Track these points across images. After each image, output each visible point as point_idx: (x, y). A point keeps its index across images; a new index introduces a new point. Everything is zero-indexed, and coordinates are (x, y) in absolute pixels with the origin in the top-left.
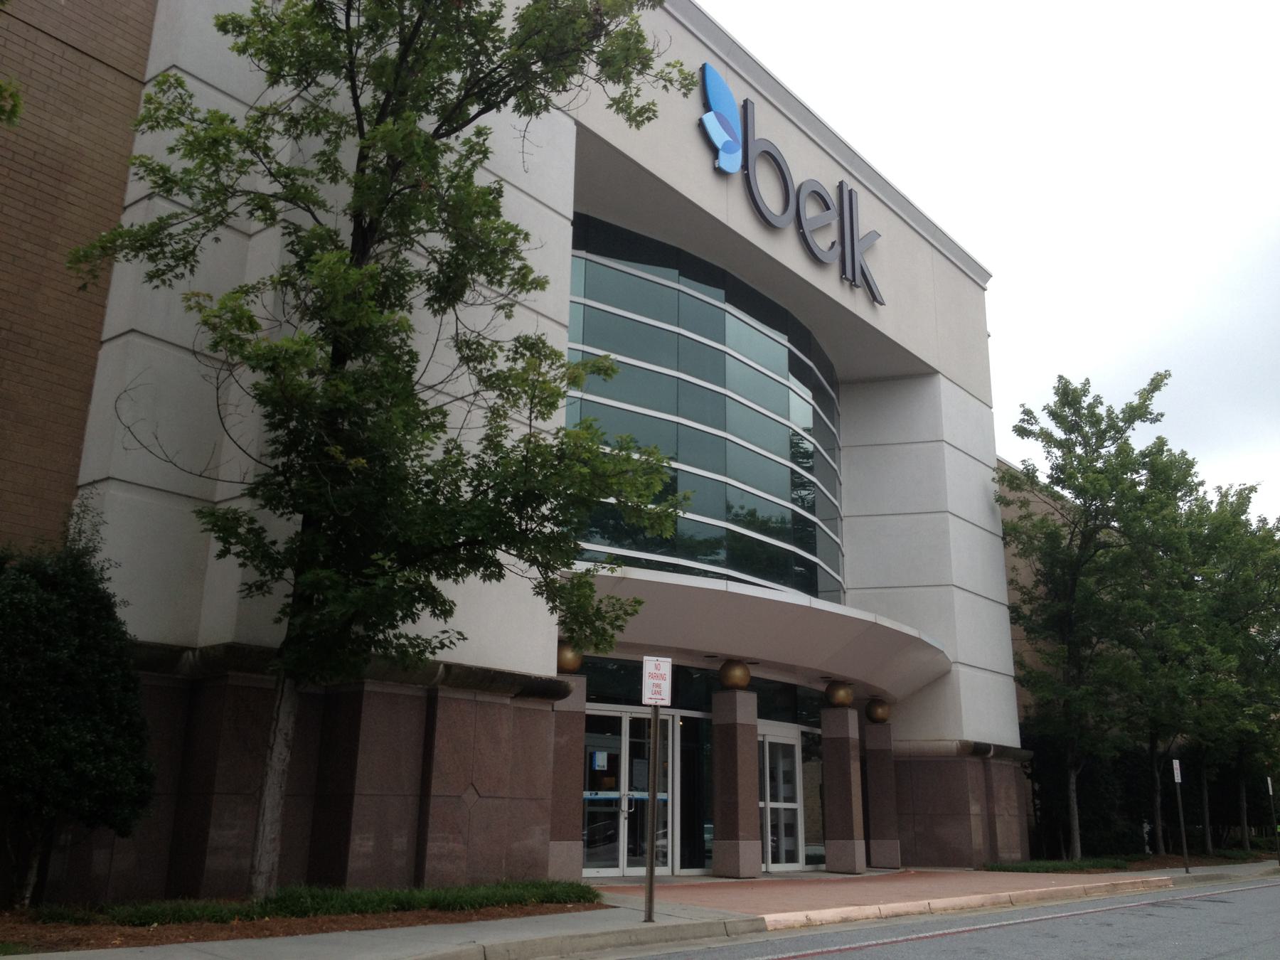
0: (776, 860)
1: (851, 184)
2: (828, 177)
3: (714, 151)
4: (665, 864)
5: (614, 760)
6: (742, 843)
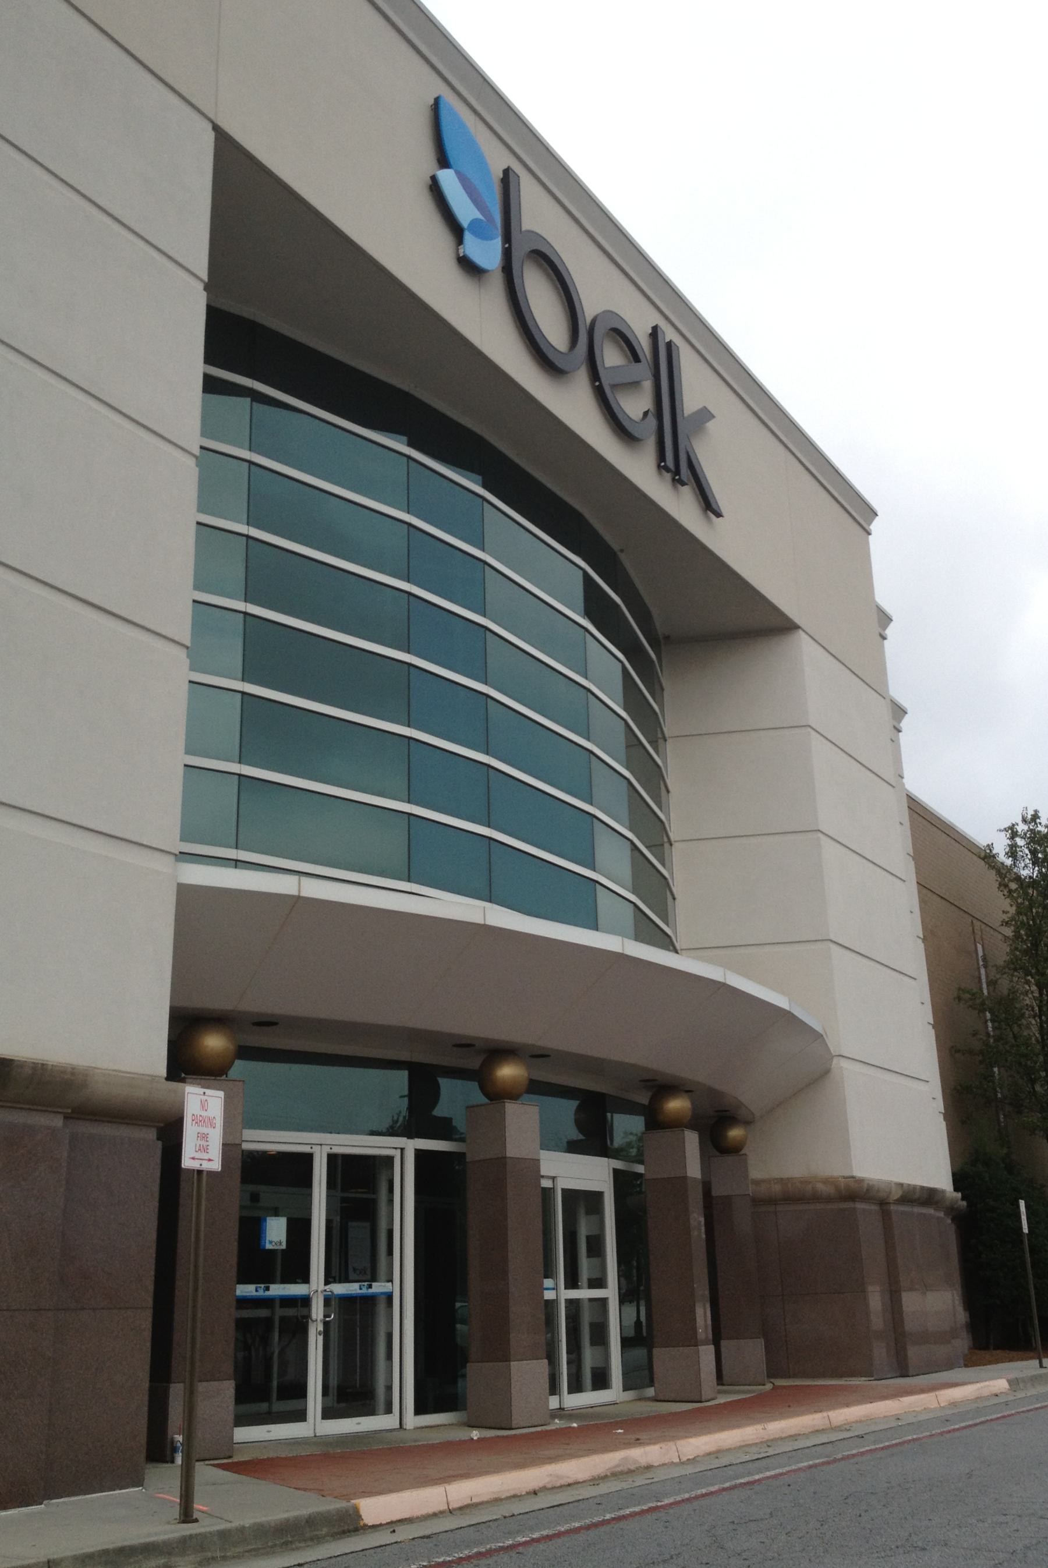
0: (576, 1387)
1: (669, 334)
3: (457, 231)
4: (389, 1410)
5: (299, 1230)
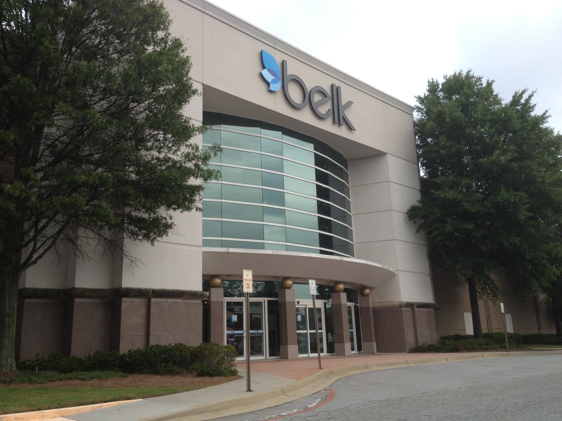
2: (326, 84)
5: (240, 317)
6: (289, 346)
